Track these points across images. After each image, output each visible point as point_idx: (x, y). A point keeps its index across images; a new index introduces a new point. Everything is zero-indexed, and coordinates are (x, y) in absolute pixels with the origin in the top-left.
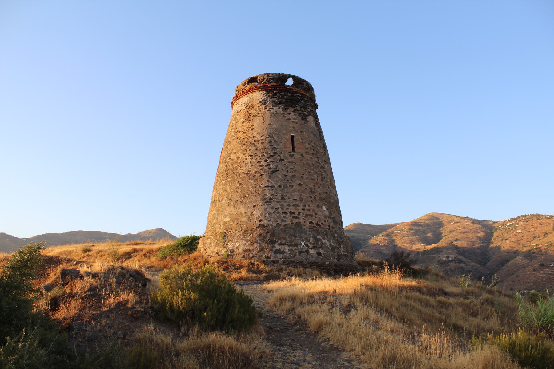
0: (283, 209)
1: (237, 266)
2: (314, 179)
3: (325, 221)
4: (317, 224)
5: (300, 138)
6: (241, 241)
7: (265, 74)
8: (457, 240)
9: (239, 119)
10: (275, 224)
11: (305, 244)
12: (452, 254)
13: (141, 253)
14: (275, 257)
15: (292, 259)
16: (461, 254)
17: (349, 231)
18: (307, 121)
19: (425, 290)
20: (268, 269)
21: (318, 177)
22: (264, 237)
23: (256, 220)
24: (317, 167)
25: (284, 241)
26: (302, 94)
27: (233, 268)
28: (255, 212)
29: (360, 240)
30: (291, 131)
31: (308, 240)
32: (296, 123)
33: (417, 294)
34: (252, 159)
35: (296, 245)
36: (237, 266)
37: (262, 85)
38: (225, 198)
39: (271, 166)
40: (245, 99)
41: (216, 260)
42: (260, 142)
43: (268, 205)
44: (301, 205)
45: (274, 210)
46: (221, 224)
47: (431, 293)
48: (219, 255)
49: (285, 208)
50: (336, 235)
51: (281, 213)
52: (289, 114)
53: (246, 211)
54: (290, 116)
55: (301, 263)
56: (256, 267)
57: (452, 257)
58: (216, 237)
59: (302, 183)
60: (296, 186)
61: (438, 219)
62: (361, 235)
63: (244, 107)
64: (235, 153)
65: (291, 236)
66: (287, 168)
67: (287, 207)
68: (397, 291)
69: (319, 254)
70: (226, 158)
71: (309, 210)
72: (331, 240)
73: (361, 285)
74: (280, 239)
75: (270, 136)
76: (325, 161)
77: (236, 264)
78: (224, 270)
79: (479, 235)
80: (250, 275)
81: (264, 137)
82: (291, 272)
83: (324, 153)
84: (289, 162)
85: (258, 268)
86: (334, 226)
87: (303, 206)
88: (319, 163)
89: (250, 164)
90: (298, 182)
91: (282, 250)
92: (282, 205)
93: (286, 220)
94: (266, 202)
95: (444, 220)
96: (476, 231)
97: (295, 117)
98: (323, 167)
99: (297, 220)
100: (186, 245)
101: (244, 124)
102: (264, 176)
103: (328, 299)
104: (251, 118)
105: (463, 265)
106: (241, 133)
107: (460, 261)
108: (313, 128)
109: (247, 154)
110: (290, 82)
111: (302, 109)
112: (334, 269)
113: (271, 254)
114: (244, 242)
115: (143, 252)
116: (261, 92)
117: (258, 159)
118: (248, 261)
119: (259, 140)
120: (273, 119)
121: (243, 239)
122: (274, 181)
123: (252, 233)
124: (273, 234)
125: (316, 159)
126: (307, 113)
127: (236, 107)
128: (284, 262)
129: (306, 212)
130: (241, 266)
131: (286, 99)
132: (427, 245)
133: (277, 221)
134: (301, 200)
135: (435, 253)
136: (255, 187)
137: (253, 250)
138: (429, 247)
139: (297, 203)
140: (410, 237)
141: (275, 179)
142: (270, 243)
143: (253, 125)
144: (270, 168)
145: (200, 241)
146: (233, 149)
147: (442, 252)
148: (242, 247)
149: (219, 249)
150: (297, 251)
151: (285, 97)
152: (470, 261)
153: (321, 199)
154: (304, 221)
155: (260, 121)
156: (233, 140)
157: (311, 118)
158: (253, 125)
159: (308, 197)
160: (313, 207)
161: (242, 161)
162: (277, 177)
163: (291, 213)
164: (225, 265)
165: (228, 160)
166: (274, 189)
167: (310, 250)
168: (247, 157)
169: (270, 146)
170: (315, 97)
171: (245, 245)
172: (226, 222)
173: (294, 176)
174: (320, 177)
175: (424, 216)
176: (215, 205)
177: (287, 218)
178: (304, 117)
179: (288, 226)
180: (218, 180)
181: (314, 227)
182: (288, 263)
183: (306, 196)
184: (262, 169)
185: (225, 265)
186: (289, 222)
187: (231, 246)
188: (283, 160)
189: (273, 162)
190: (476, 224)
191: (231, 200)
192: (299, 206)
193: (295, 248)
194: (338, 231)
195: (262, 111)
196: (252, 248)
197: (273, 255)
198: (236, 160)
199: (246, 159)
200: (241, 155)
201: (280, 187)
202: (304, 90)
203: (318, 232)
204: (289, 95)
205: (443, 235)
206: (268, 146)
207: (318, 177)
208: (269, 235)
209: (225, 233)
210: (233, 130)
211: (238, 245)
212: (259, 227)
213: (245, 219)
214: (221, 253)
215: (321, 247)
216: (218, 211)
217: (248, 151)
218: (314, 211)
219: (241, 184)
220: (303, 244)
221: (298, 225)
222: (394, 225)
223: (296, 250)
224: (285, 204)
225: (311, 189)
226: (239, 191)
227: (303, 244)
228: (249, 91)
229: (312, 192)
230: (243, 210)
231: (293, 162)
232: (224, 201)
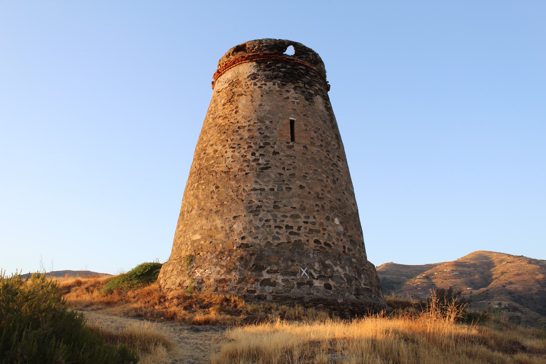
0: (275, 221)
1: (205, 303)
2: (321, 180)
3: (338, 240)
4: (326, 244)
5: (302, 123)
6: (213, 267)
7: (255, 40)
8: (511, 283)
9: (219, 100)
10: (263, 243)
11: (306, 271)
12: (505, 300)
13: (83, 287)
14: (262, 290)
15: (287, 294)
16: (516, 301)
17: (382, 273)
18: (313, 102)
19: (492, 342)
20: (250, 308)
21: (328, 177)
22: (247, 261)
23: (236, 237)
24: (327, 164)
25: (275, 268)
26: (307, 67)
27: (198, 306)
28: (235, 226)
29: (394, 283)
30: (289, 115)
31: (311, 266)
32: (298, 103)
33: (483, 349)
34: (233, 152)
35: (294, 273)
36: (205, 303)
37: (250, 54)
38: (196, 207)
39: (261, 161)
40: (229, 75)
41: (176, 295)
42: (246, 128)
43: (255, 215)
44: (303, 216)
45: (263, 222)
46: (189, 244)
47: (500, 346)
48: (182, 288)
49: (278, 220)
50: (354, 260)
51: (273, 226)
52: (288, 91)
53: (223, 225)
54: (289, 94)
55: (300, 300)
56: (233, 305)
57: (505, 303)
58: (181, 261)
59: (304, 185)
60: (295, 190)
61: (486, 257)
62: (395, 277)
63: (227, 85)
64: (212, 145)
65: (286, 260)
66: (283, 163)
67: (282, 218)
68: (452, 343)
69: (328, 287)
70: (201, 152)
71: (314, 224)
72: (347, 268)
73: (387, 332)
74: (270, 264)
75: (261, 120)
76: (338, 157)
77: (204, 300)
78: (185, 308)
79: (537, 277)
80: (220, 317)
81: (252, 123)
82: (285, 313)
83: (337, 146)
84: (287, 156)
85: (236, 306)
86: (352, 248)
87: (305, 217)
88: (330, 159)
89: (231, 160)
90: (299, 183)
91: (272, 281)
92: (275, 216)
93: (280, 236)
94: (251, 212)
95: (495, 260)
96: (533, 273)
97: (296, 96)
98: (335, 165)
99: (297, 238)
100: (142, 275)
101: (226, 106)
102: (250, 175)
103: (317, 357)
104: (236, 98)
105: (519, 314)
106: (221, 118)
107: (515, 309)
108: (322, 111)
109: (227, 146)
110: (290, 51)
111: (307, 86)
112: (350, 310)
113: (257, 287)
114: (218, 268)
115: (86, 285)
116: (250, 64)
117: (243, 151)
118: (222, 296)
119: (245, 127)
120: (265, 98)
121: (216, 265)
122: (264, 182)
123: (230, 255)
124: (260, 257)
125: (325, 153)
126: (313, 92)
127: (218, 87)
128: (275, 298)
129: (310, 226)
130: (211, 303)
131: (285, 72)
132: (474, 289)
133: (267, 238)
134: (303, 209)
135: (484, 299)
136: (237, 191)
137: (230, 280)
138: (475, 292)
139: (297, 212)
140: (453, 280)
141: (266, 180)
142: (255, 270)
143: (237, 107)
144: (259, 164)
145: (162, 270)
146: (210, 141)
147: (493, 297)
148: (214, 276)
149: (183, 279)
150: (295, 283)
151: (283, 70)
152: (527, 309)
153: (332, 209)
154: (306, 238)
155: (247, 101)
156: (210, 128)
157: (319, 99)
158: (237, 107)
159: (312, 205)
160: (320, 219)
161: (220, 155)
162: (269, 176)
163: (287, 227)
164: (188, 302)
165: (202, 155)
166: (264, 193)
167: (314, 281)
168: (228, 150)
169: (260, 133)
170: (325, 72)
171: (218, 272)
172: (194, 241)
173: (293, 175)
174: (331, 178)
175: (469, 255)
176: (183, 218)
177: (282, 234)
178: (309, 97)
179: (284, 245)
180: (189, 184)
181: (321, 247)
182: (280, 299)
183: (310, 203)
184: (248, 166)
185: (188, 302)
186: (283, 240)
187: (198, 274)
188: (278, 153)
189: (263, 155)
190: (533, 264)
191: (203, 209)
192: (300, 217)
193: (292, 277)
194: (357, 255)
195: (251, 89)
196: (228, 277)
197: (259, 287)
198: (212, 154)
199: (226, 152)
200: (220, 148)
201: (272, 190)
202: (310, 61)
203: (327, 254)
204: (288, 66)
205: (494, 277)
206: (257, 134)
207: (328, 177)
208: (253, 258)
209: (193, 256)
210: (212, 116)
211: (209, 273)
212: (240, 247)
213: (220, 236)
214: (185, 285)
215: (331, 277)
216: (185, 225)
217: (230, 142)
218: (321, 224)
219: (217, 187)
220: (304, 272)
221: (298, 244)
222: (435, 265)
223: (294, 280)
224: (279, 215)
225: (317, 194)
226: (215, 197)
227: (304, 272)
228: (234, 63)
229: (318, 197)
230: (219, 223)
231: (291, 156)
232: (194, 212)
